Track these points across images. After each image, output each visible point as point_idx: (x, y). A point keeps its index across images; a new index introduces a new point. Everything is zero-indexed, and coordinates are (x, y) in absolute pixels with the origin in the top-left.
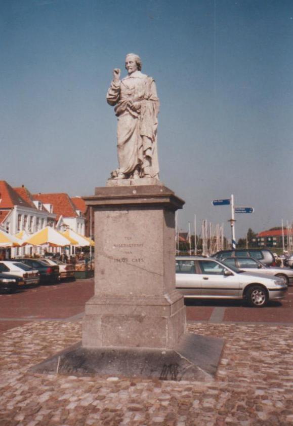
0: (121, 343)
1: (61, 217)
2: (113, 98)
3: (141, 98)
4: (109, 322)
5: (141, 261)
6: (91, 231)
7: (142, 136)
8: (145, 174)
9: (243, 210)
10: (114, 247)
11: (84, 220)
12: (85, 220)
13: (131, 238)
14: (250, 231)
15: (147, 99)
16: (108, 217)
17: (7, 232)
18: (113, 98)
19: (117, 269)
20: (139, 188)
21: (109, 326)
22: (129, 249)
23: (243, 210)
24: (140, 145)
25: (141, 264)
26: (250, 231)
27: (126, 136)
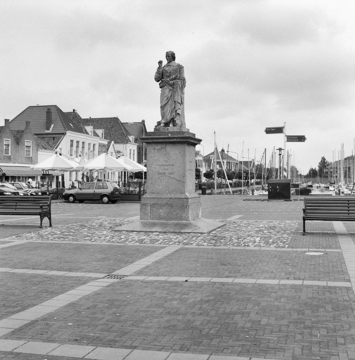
0: (161, 218)
1: (113, 142)
2: (158, 78)
3: (175, 79)
4: (155, 207)
5: (173, 174)
6: (144, 157)
7: (175, 102)
8: (177, 124)
9: (296, 139)
10: (158, 166)
11: (136, 146)
12: (137, 146)
13: (167, 161)
14: (323, 159)
15: (178, 79)
16: (155, 149)
17: (112, 155)
18: (158, 78)
19: (159, 179)
20: (172, 133)
21: (154, 209)
22: (166, 167)
23: (296, 139)
24: (173, 107)
25: (173, 176)
26: (323, 159)
27: (165, 101)
